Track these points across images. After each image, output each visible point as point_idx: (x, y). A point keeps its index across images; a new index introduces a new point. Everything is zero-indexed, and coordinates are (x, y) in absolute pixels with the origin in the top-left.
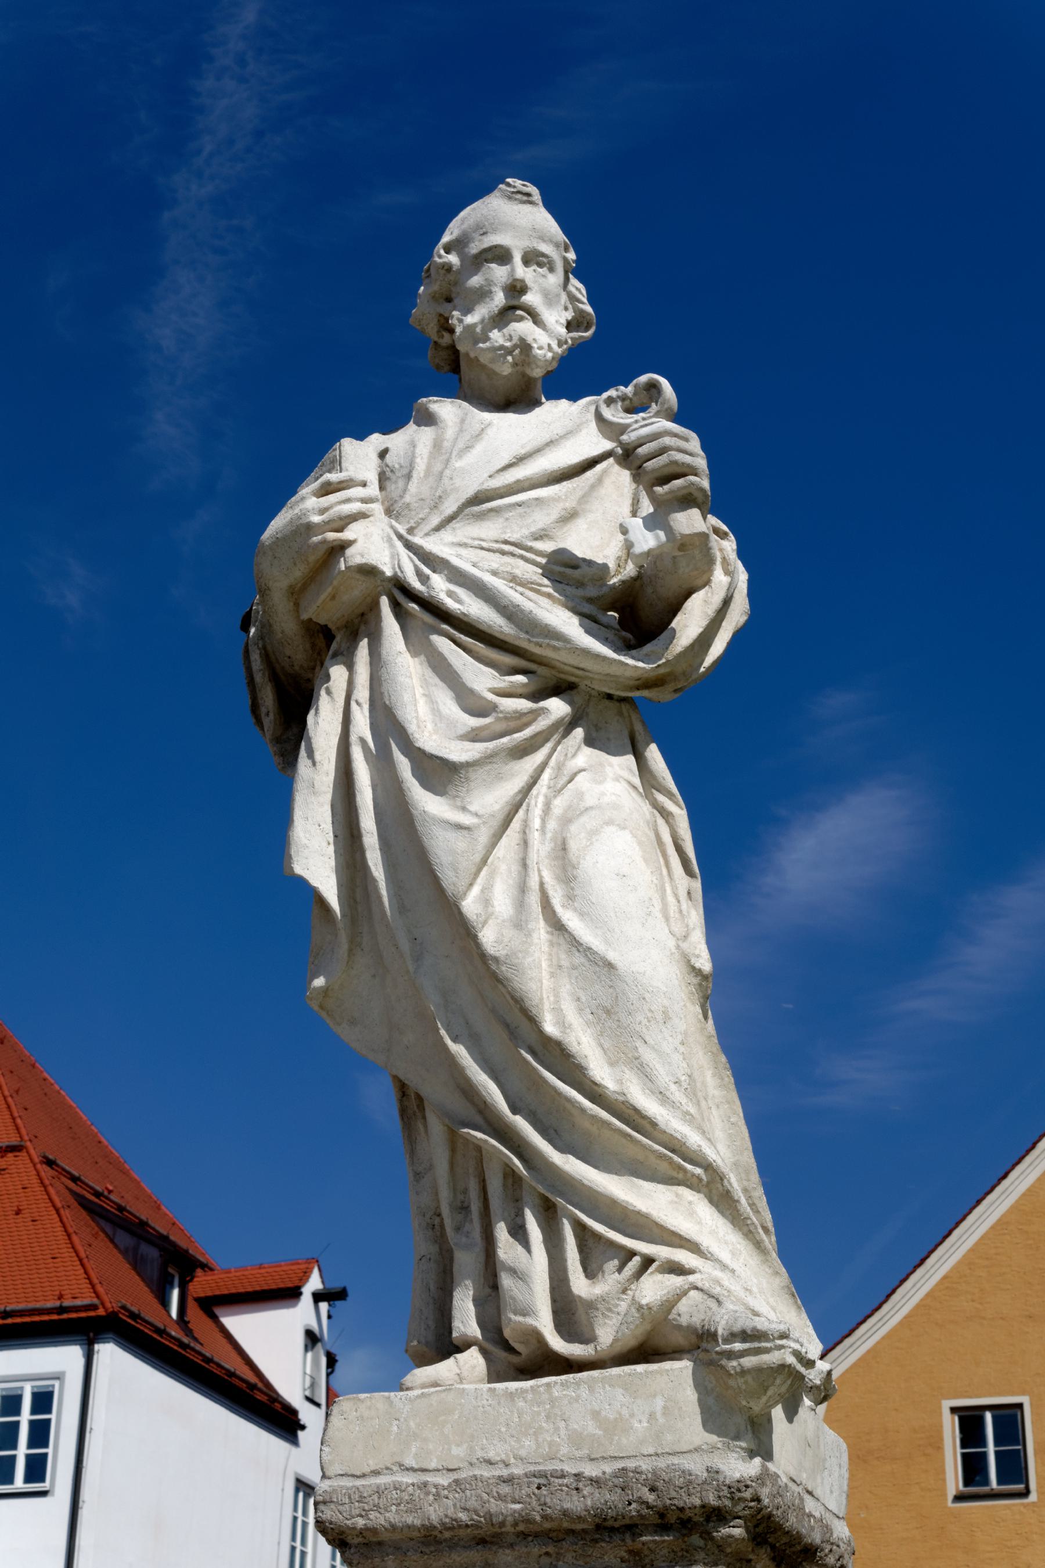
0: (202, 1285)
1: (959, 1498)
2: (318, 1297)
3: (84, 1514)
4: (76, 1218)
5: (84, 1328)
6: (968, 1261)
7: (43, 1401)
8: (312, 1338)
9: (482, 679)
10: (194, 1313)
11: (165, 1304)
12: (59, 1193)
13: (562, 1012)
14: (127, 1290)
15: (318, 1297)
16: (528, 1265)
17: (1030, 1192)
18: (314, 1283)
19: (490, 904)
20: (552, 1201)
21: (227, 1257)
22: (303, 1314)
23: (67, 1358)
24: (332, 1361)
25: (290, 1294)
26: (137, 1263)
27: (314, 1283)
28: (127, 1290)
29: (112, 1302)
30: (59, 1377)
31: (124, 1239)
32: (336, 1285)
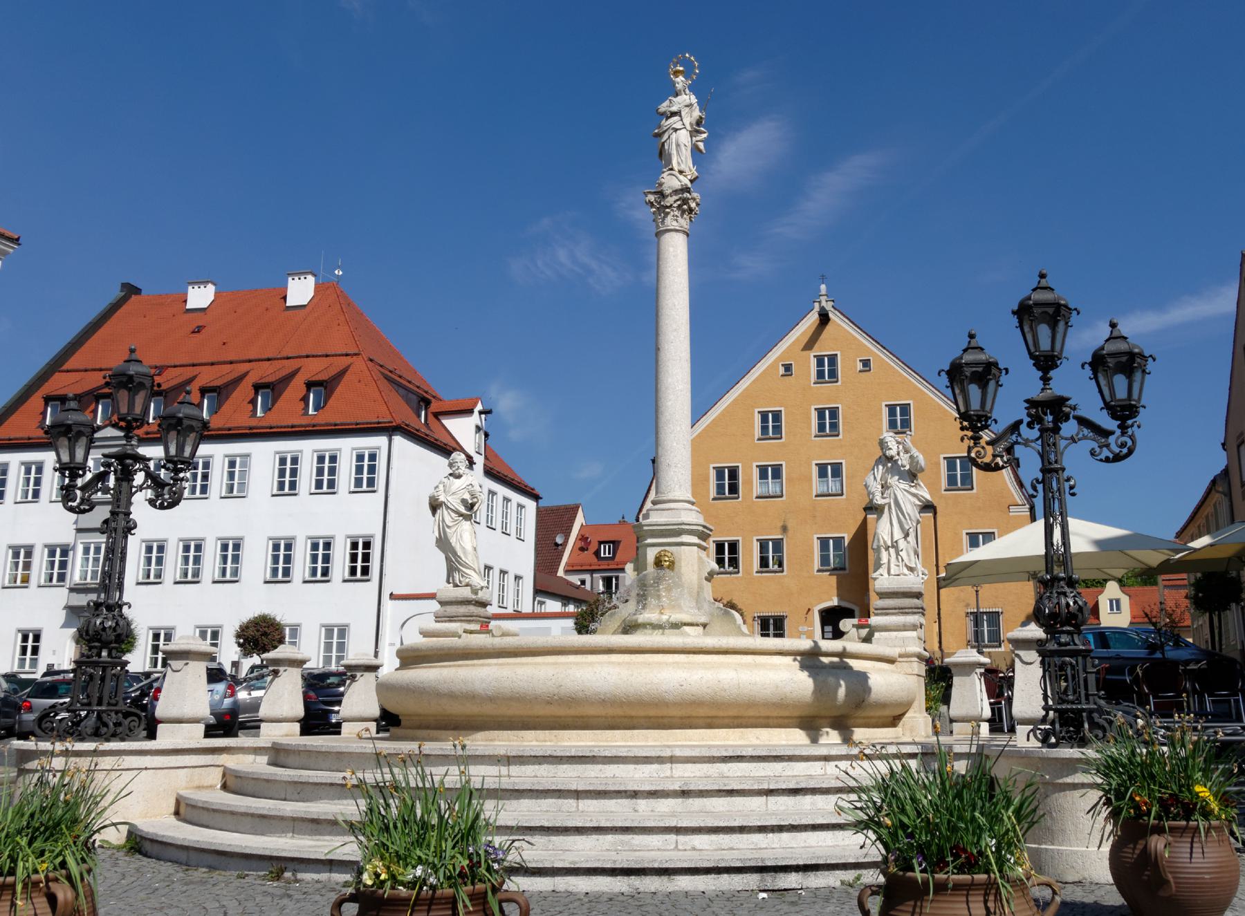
0: (434, 407)
1: (714, 499)
2: (480, 413)
3: (390, 499)
4: (384, 384)
5: (389, 430)
6: (723, 414)
7: (373, 457)
8: (478, 429)
9: (453, 515)
10: (431, 417)
11: (419, 416)
12: (377, 375)
13: (460, 553)
14: (403, 414)
15: (480, 413)
16: (457, 576)
17: (746, 389)
18: (479, 407)
19: (453, 541)
20: (459, 570)
21: (447, 394)
22: (475, 419)
23: (380, 441)
24: (486, 435)
25: (469, 412)
26: (408, 402)
27: (479, 407)
28: (403, 414)
29: (399, 421)
30: (379, 448)
31: (402, 391)
32: (488, 408)
